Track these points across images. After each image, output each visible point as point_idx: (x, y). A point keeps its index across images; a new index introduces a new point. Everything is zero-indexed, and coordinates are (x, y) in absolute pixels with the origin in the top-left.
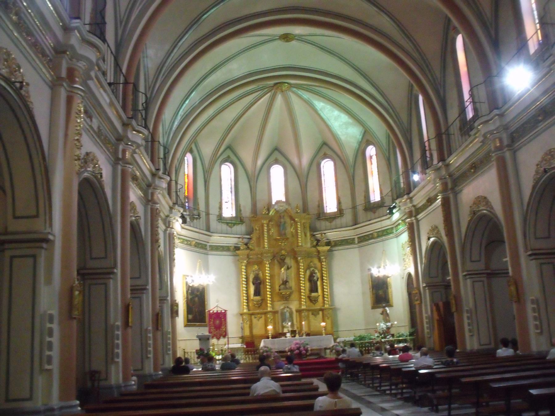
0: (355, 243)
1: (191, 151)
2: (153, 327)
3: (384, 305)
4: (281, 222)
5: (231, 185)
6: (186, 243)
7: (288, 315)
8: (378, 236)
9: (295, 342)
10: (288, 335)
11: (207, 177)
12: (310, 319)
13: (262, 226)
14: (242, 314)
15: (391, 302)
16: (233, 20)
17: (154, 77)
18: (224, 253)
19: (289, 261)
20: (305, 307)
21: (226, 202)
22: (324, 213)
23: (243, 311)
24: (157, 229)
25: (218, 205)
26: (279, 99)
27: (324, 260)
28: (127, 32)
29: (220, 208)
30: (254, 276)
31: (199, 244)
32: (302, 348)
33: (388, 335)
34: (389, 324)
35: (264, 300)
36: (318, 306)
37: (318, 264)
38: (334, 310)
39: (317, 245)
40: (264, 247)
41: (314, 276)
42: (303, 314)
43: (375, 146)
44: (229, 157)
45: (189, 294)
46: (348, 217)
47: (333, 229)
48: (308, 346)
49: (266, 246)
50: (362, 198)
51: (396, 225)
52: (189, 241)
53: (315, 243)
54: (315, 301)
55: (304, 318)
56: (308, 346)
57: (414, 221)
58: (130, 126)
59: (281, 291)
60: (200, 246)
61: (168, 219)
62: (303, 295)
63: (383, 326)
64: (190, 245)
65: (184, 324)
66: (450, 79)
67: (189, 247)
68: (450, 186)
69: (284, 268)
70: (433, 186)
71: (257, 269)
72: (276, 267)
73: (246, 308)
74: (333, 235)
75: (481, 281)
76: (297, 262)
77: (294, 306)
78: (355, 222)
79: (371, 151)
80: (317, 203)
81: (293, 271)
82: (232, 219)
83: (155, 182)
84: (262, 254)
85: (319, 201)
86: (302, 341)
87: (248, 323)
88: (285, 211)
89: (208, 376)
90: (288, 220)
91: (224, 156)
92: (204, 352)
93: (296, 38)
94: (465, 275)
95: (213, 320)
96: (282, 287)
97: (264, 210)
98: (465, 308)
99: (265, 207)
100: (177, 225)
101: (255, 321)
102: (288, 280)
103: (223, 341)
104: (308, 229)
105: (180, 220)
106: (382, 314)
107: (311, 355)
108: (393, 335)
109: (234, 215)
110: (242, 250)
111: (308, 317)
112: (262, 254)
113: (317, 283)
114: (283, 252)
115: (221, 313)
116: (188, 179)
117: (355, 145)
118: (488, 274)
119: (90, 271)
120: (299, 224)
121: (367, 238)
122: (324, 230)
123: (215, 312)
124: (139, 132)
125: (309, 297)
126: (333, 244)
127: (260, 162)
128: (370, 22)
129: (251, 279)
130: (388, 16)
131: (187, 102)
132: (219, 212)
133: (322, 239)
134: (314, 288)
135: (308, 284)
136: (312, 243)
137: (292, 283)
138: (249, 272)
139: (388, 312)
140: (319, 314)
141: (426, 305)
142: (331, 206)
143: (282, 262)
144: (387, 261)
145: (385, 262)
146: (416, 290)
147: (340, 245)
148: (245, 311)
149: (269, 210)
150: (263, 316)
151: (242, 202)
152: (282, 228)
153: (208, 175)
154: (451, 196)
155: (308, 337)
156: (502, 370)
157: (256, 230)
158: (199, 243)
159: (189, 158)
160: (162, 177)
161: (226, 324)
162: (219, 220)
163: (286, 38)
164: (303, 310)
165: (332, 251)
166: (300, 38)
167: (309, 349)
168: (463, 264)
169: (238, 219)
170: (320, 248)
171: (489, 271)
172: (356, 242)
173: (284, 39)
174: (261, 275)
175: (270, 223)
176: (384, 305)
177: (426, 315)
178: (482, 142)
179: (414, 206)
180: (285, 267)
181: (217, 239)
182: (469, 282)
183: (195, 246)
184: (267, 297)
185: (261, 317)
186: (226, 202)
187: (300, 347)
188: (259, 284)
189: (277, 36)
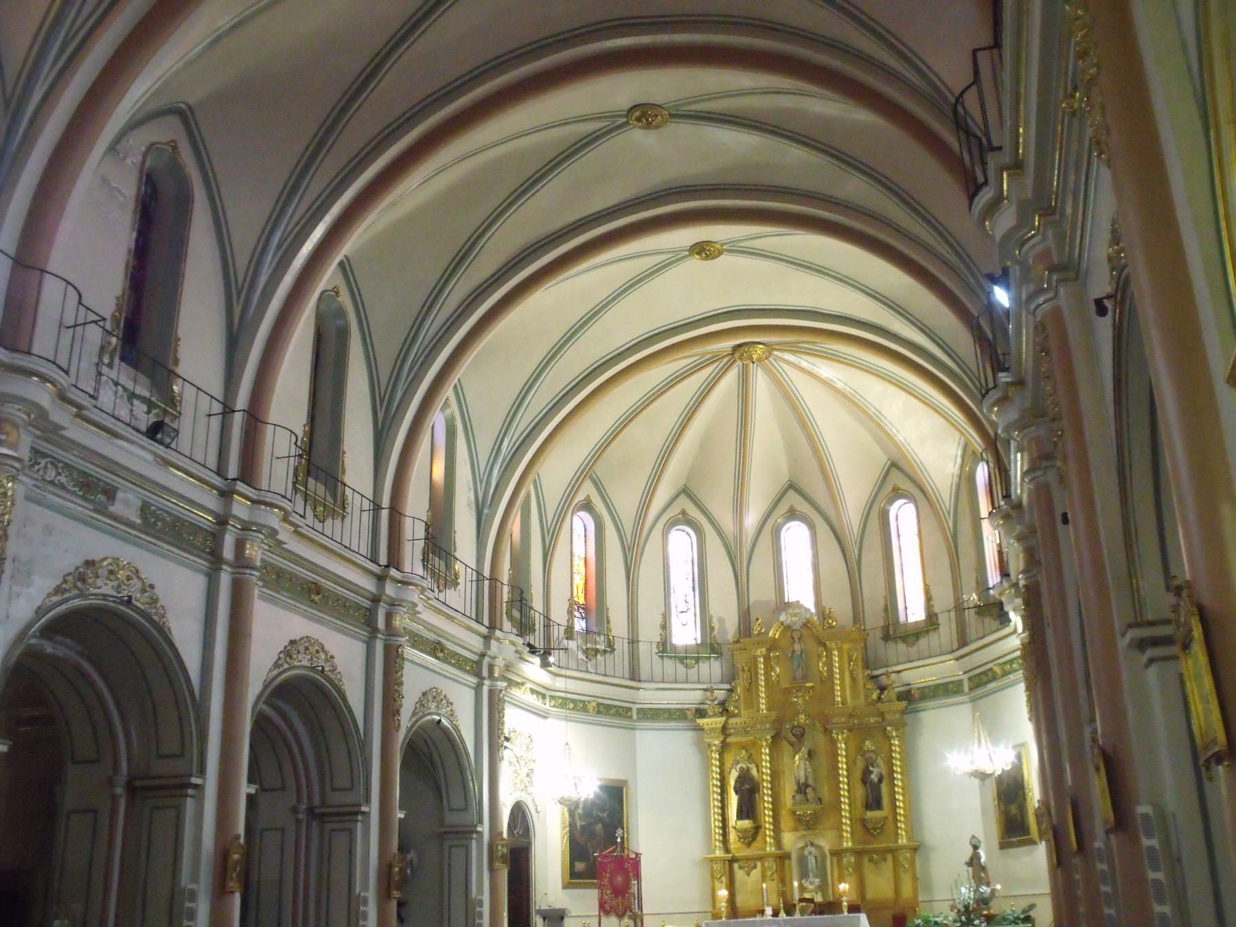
0: (963, 691)
1: (587, 506)
6: (572, 705)
7: (812, 860)
13: (754, 660)
14: (711, 860)
16: (552, 235)
18: (673, 724)
19: (816, 739)
20: (850, 844)
21: (682, 612)
25: (659, 620)
26: (761, 383)
27: (894, 734)
28: (253, 308)
29: (665, 626)
31: (608, 707)
41: (872, 772)
42: (845, 860)
44: (684, 512)
46: (946, 631)
52: (583, 702)
53: (875, 696)
61: (486, 660)
64: (584, 709)
65: (563, 882)
74: (920, 675)
78: (963, 643)
80: (882, 603)
81: (823, 760)
82: (687, 649)
87: (724, 879)
90: (812, 645)
91: (674, 511)
95: (608, 875)
99: (758, 619)
101: (739, 874)
104: (860, 664)
119: (155, 783)
127: (751, 520)
129: (732, 782)
134: (874, 802)
135: (860, 791)
136: (867, 697)
138: (728, 765)
139: (982, 860)
140: (885, 859)
142: (913, 610)
147: (932, 697)
148: (848, 844)
151: (715, 610)
162: (660, 652)
163: (702, 250)
164: (846, 850)
169: (711, 647)
172: (966, 689)
173: (699, 253)
174: (754, 772)
180: (804, 750)
181: (650, 696)
183: (599, 712)
185: (755, 867)
186: (682, 612)
188: (748, 792)
189: (686, 250)
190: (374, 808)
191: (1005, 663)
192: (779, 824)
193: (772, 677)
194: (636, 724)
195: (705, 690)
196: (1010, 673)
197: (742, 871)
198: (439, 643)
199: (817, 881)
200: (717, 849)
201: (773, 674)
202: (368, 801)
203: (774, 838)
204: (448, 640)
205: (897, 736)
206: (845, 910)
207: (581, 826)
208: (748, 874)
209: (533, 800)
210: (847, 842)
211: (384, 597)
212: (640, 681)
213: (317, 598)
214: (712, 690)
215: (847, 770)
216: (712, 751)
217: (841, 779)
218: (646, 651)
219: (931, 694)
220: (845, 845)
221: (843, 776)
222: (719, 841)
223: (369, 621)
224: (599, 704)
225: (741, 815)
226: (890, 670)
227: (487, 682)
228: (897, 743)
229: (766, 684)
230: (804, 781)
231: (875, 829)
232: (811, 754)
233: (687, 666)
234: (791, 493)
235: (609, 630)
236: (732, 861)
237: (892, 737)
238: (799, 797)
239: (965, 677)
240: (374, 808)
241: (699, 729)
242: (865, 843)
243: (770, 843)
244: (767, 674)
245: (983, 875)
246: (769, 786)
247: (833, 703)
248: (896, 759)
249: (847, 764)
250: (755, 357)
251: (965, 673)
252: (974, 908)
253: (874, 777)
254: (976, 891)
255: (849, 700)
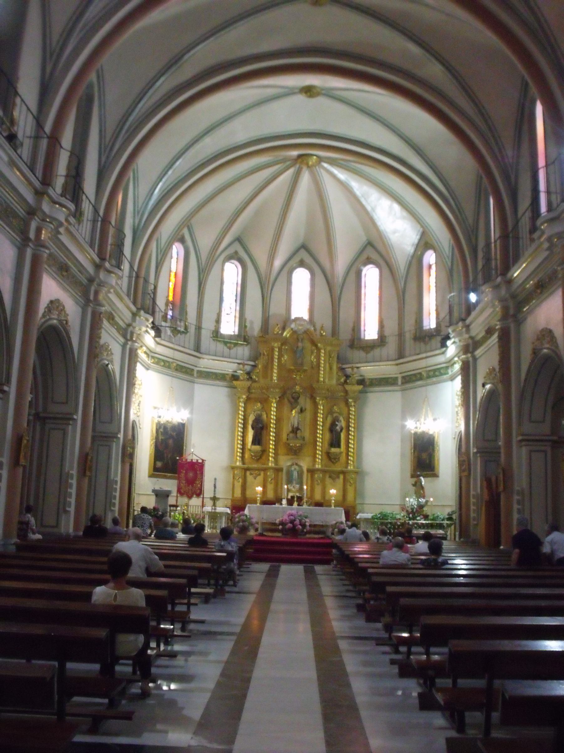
1: (182, 240)
2: (78, 472)
3: (419, 473)
4: (298, 347)
5: (237, 291)
6: (162, 364)
7: (295, 474)
8: (429, 377)
9: (289, 512)
10: (284, 502)
11: (203, 278)
12: (326, 483)
13: (273, 350)
14: (233, 468)
15: (436, 470)
17: (113, 135)
18: (218, 382)
19: (304, 402)
20: (320, 466)
22: (359, 339)
23: (235, 464)
24: (97, 340)
25: (215, 317)
26: (305, 178)
27: (353, 404)
30: (254, 417)
31: (182, 367)
32: (297, 522)
33: (418, 516)
34: (422, 500)
35: (264, 452)
36: (338, 467)
37: (345, 410)
38: (359, 473)
39: (345, 382)
40: (272, 379)
41: (337, 425)
42: (316, 476)
43: (435, 252)
44: (236, 253)
45: (160, 433)
46: (391, 348)
47: (369, 362)
48: (307, 520)
49: (275, 378)
50: (413, 321)
51: (450, 363)
52: (168, 362)
53: (342, 380)
54: (335, 459)
55: (317, 481)
56: (307, 520)
57: (471, 359)
58: (45, 196)
59: (289, 442)
60: (184, 370)
61: (130, 329)
62: (319, 450)
63: (412, 501)
64: (169, 367)
66: (525, 161)
67: (165, 370)
68: (512, 312)
69: (296, 409)
70: (493, 311)
71: (260, 408)
72: (286, 409)
73: (239, 460)
75: (541, 451)
76: (315, 405)
77: (305, 464)
78: (401, 355)
79: (430, 257)
81: (308, 415)
82: (231, 337)
83: (99, 276)
84: (268, 389)
85: (354, 323)
86: (300, 513)
87: (240, 480)
88: (306, 332)
89: (178, 546)
90: (308, 345)
92: (157, 513)
93: (323, 92)
94: (521, 441)
95: (184, 472)
96: (291, 435)
97: (277, 329)
98: (517, 488)
99: (277, 325)
100: (149, 339)
101: (250, 478)
102: (300, 427)
103: (195, 501)
104: (335, 359)
105: (153, 333)
106: (414, 485)
107: (309, 532)
108: (426, 517)
109: (237, 333)
110: (242, 380)
111: (323, 481)
112: (268, 389)
113: (340, 435)
114: (298, 388)
115: (198, 462)
116: (175, 277)
117: (410, 249)
118: (554, 442)
120: (323, 351)
121: (414, 379)
122: (357, 363)
123: (189, 460)
124: (62, 205)
125: (328, 455)
126: (367, 383)
127: (277, 263)
128: (421, 73)
129: (250, 422)
130: (443, 65)
131: (170, 172)
132: (215, 326)
133: (353, 375)
134: (335, 442)
135: (328, 436)
136: (338, 379)
137: (306, 433)
138: (249, 411)
139: (423, 483)
140: (338, 477)
141: (475, 480)
143: (294, 401)
144: (429, 412)
145: (427, 412)
146: (463, 456)
148: (318, 466)
149: (284, 329)
150: (262, 473)
151: (249, 315)
152: (298, 355)
153: (204, 276)
154: (512, 326)
155: (317, 508)
156: (520, 580)
157: (264, 354)
158: (182, 366)
159: (177, 250)
160: (111, 270)
161: (202, 478)
162: (214, 337)
163: (309, 91)
164: (318, 470)
165: (366, 392)
166: (329, 94)
167: (307, 524)
168: (520, 424)
170: (348, 387)
171: (555, 438)
173: (306, 92)
174: (264, 416)
175: (283, 347)
176: (419, 473)
177: (474, 493)
178: (549, 249)
179: (472, 338)
180: (298, 408)
182: (524, 450)
183: (177, 370)
184: (270, 448)
185: (259, 475)
187: (295, 520)
190: (79, 417)
191: (430, 371)
192: (278, 450)
193: (282, 360)
194: (196, 380)
195: (239, 364)
196: (433, 377)
197: (251, 476)
198: (112, 314)
199: (298, 486)
200: (238, 461)
201: (283, 359)
202: (76, 412)
203: (274, 458)
204: (116, 313)
205: (354, 406)
206: (333, 505)
207: (162, 439)
208: (255, 478)
209: (139, 421)
210: (318, 465)
211: (97, 280)
212: (201, 353)
213: (65, 274)
214: (244, 365)
215: (323, 422)
216: (240, 402)
217: (318, 427)
218: (206, 334)
219: (377, 383)
220: (317, 466)
221: (320, 425)
222: (239, 456)
223: (85, 293)
224: (178, 365)
225: (254, 442)
226: (354, 365)
227: (130, 343)
228: (353, 409)
229: (278, 364)
230: (297, 426)
231: (335, 459)
232: (302, 411)
233: (230, 348)
234: (302, 251)
235: (186, 319)
236: (246, 470)
237: (351, 406)
238: (291, 435)
239: (400, 376)
240: (79, 417)
241: (234, 387)
242: (326, 466)
243: (272, 461)
244: (279, 359)
245: (422, 492)
246: (274, 427)
247: (318, 381)
248: (352, 419)
249: (323, 418)
250: (310, 163)
251: (400, 373)
252: (416, 511)
253: (338, 428)
254: (418, 500)
255: (327, 380)
